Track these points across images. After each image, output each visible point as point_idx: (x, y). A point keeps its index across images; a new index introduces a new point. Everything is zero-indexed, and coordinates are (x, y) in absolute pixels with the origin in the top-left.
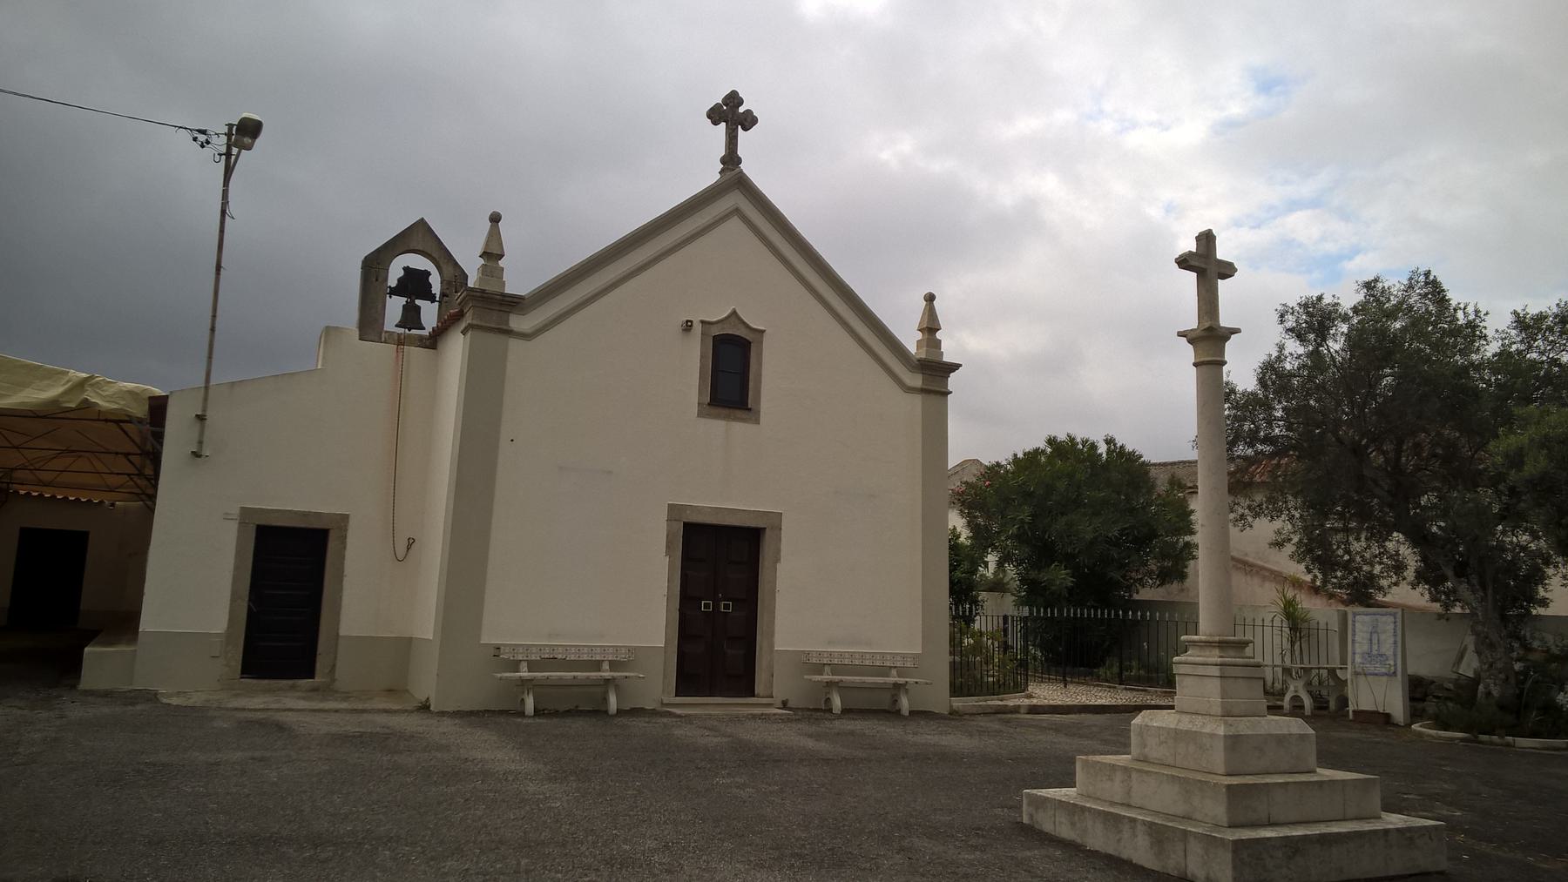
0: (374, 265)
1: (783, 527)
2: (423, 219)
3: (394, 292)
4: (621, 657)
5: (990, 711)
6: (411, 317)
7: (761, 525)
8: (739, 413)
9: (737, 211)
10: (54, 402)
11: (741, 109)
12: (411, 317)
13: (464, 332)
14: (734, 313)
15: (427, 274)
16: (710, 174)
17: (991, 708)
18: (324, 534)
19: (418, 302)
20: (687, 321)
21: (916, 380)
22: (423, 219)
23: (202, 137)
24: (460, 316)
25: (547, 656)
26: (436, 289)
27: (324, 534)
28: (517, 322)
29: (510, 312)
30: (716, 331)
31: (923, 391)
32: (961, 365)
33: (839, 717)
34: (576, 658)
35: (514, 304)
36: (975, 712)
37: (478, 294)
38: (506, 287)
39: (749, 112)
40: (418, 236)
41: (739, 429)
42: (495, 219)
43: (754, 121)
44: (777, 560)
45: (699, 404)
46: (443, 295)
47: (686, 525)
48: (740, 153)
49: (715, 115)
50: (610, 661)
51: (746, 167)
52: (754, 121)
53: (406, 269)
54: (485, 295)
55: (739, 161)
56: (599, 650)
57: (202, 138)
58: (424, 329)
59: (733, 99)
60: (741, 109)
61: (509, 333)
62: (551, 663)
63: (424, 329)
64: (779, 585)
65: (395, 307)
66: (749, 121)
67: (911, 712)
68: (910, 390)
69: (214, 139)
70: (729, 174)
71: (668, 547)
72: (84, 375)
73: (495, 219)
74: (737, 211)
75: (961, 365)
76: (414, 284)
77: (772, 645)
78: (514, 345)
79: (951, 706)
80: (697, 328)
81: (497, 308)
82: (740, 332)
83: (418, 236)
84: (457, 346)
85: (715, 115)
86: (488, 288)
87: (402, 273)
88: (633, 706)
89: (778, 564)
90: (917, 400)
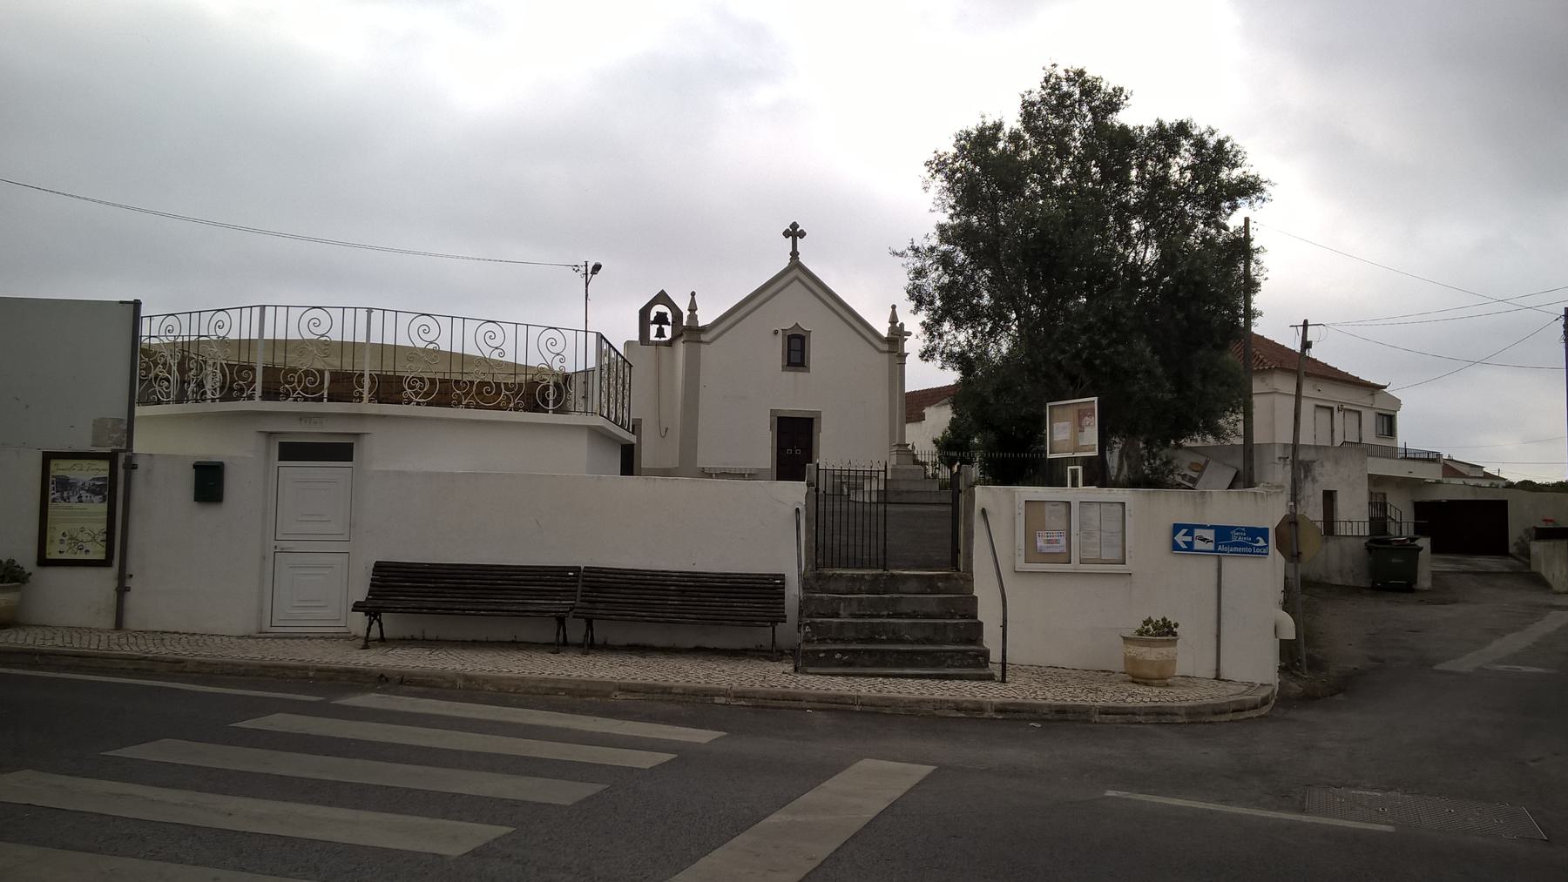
0: (644, 313)
2: (663, 291)
3: (653, 323)
6: (660, 333)
8: (801, 368)
9: (797, 278)
12: (660, 333)
13: (683, 342)
15: (666, 314)
16: (785, 262)
18: (781, 420)
19: (663, 326)
21: (886, 347)
22: (663, 291)
23: (576, 268)
24: (681, 335)
26: (670, 320)
27: (810, 421)
28: (704, 337)
30: (789, 333)
35: (704, 329)
38: (698, 461)
39: (802, 231)
40: (662, 298)
41: (801, 375)
43: (805, 234)
44: (820, 431)
46: (673, 322)
47: (778, 418)
49: (786, 234)
51: (802, 259)
52: (805, 234)
53: (657, 312)
57: (576, 268)
58: (664, 337)
59: (794, 226)
61: (701, 342)
63: (664, 337)
65: (654, 329)
66: (802, 235)
69: (581, 268)
70: (794, 261)
74: (797, 278)
76: (661, 318)
78: (702, 345)
80: (780, 333)
83: (662, 298)
84: (680, 347)
85: (786, 234)
86: (692, 325)
87: (656, 314)
90: (886, 356)
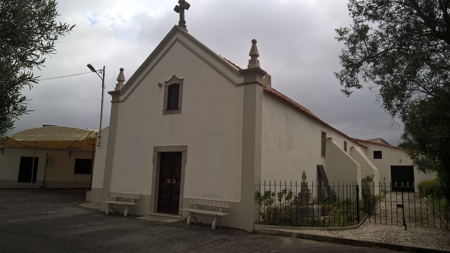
4: (137, 198)
5: (274, 233)
7: (181, 151)
8: (175, 111)
10: (86, 137)
17: (275, 232)
20: (159, 83)
21: (241, 80)
25: (119, 197)
30: (169, 84)
31: (244, 84)
32: (108, 92)
33: (126, 217)
34: (128, 198)
48: (186, 19)
50: (134, 199)
55: (185, 22)
60: (179, 5)
64: (186, 174)
67: (192, 223)
68: (238, 85)
71: (153, 161)
72: (92, 130)
77: (183, 196)
79: (254, 229)
81: (116, 95)
89: (186, 165)
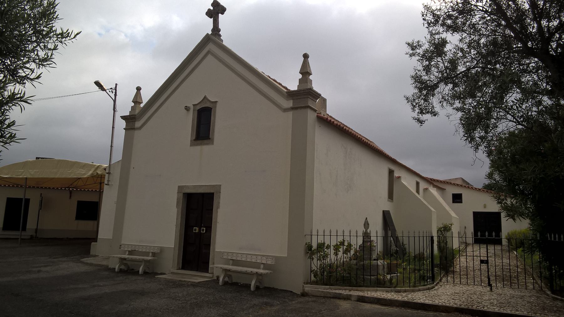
1: (221, 191)
5: (329, 295)
7: (212, 191)
8: (205, 141)
10: (92, 174)
11: (212, 8)
14: (205, 97)
20: (185, 107)
21: (289, 104)
29: (135, 121)
30: (198, 107)
31: (293, 109)
36: (319, 295)
37: (302, 92)
42: (306, 56)
45: (191, 141)
50: (152, 252)
54: (126, 117)
56: (148, 248)
60: (212, 8)
62: (236, 263)
68: (285, 110)
72: (99, 165)
73: (306, 56)
75: (121, 117)
77: (214, 249)
78: (136, 132)
79: (304, 290)
82: (208, 105)
88: (162, 272)
89: (218, 209)
